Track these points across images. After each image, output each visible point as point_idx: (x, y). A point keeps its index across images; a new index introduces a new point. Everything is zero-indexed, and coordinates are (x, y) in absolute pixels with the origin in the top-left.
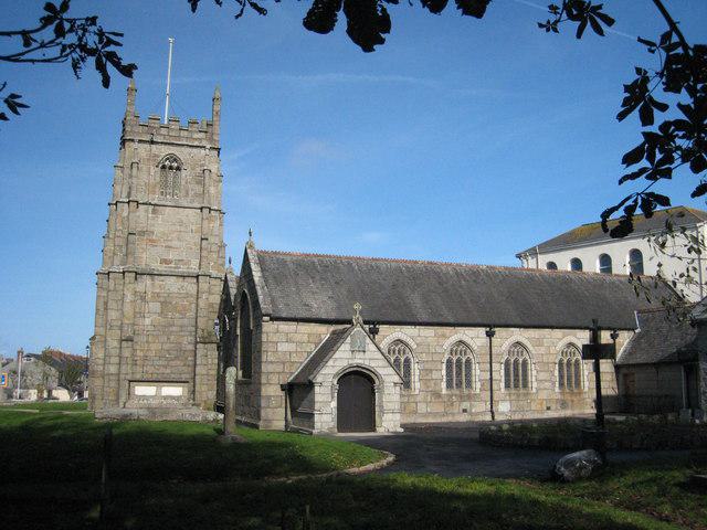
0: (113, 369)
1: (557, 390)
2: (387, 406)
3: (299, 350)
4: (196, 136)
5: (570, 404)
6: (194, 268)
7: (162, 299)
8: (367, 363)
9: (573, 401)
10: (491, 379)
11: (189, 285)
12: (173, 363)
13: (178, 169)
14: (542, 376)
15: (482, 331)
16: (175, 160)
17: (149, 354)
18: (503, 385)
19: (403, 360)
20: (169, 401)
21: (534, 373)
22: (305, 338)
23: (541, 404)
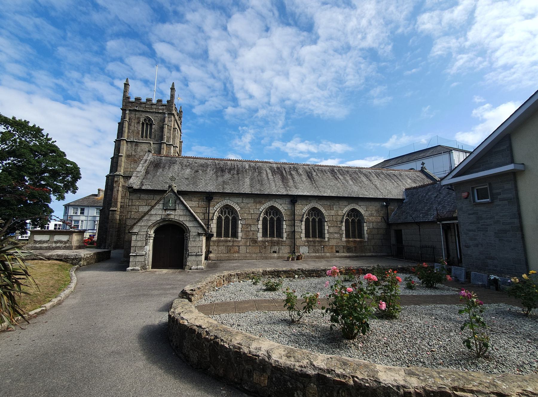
1: (344, 239)
4: (160, 108)
14: (332, 230)
18: (303, 235)
19: (230, 218)
21: (326, 228)
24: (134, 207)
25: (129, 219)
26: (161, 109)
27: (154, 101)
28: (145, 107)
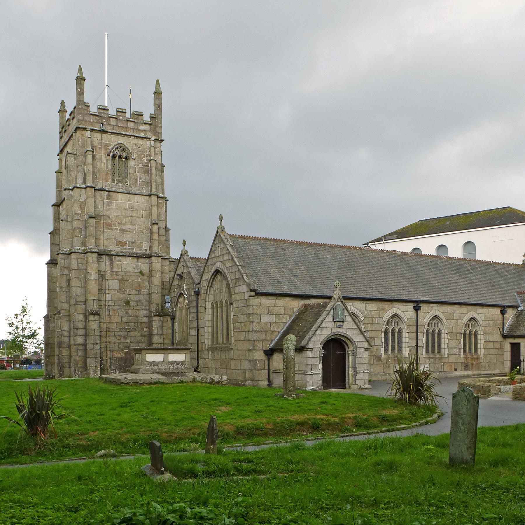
0: (80, 340)
1: (462, 355)
2: (508, 369)
3: (277, 321)
4: (141, 127)
5: (470, 366)
6: (145, 249)
7: (120, 277)
8: (345, 331)
9: (472, 364)
10: (417, 345)
11: (143, 265)
12: (132, 334)
13: (127, 158)
14: (453, 343)
15: (411, 306)
16: (123, 150)
17: (111, 326)
18: (424, 350)
20: (175, 366)
22: (282, 311)
23: (451, 366)
24: (255, 316)
25: (252, 331)
26: (142, 131)
27: (112, 112)
28: (117, 125)
